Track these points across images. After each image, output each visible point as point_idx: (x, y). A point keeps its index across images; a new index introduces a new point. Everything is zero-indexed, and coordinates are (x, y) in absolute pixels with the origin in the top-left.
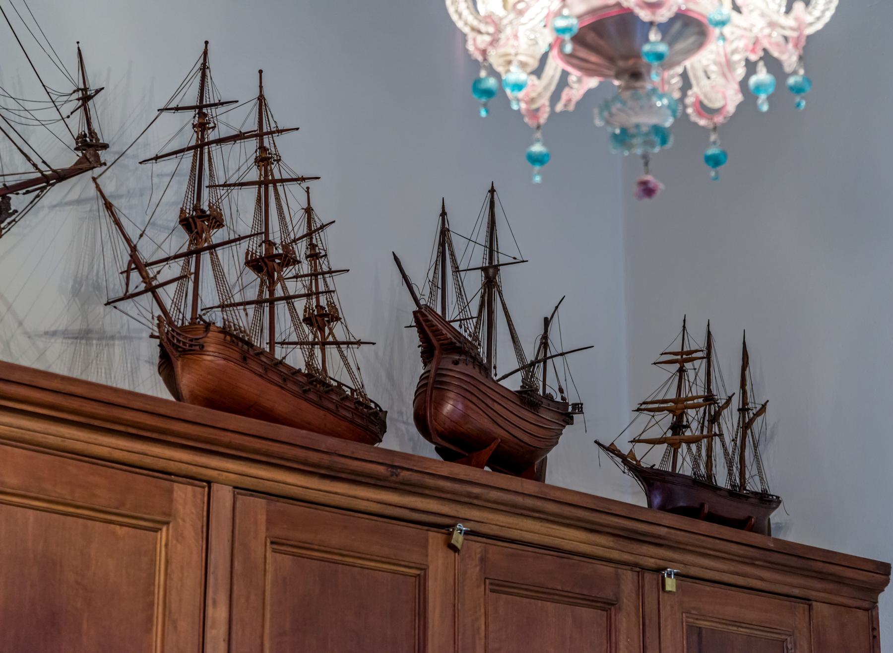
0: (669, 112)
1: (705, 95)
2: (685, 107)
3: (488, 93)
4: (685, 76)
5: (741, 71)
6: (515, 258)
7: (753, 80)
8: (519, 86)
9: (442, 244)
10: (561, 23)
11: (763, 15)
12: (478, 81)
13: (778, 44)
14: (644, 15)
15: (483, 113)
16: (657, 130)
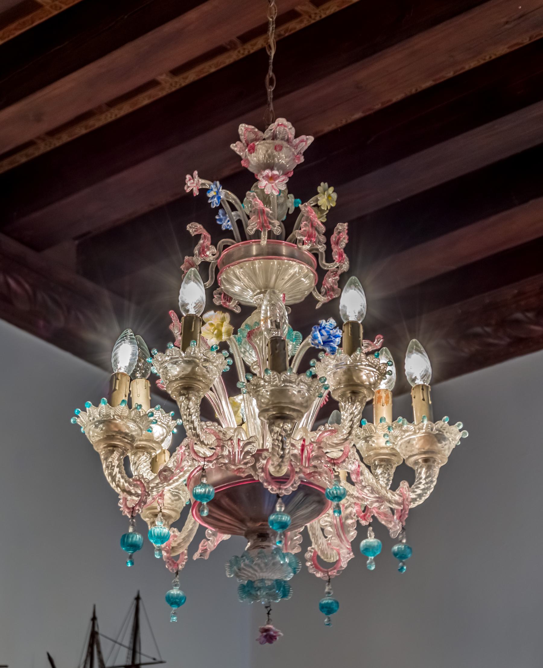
0: (290, 569)
1: (322, 551)
2: (304, 561)
3: (134, 547)
4: (305, 534)
5: (353, 533)
6: (154, 659)
7: (363, 543)
8: (162, 538)
9: (91, 646)
10: (200, 490)
11: (373, 491)
12: (126, 536)
13: (385, 515)
14: (272, 489)
15: (129, 565)
16: (280, 584)
